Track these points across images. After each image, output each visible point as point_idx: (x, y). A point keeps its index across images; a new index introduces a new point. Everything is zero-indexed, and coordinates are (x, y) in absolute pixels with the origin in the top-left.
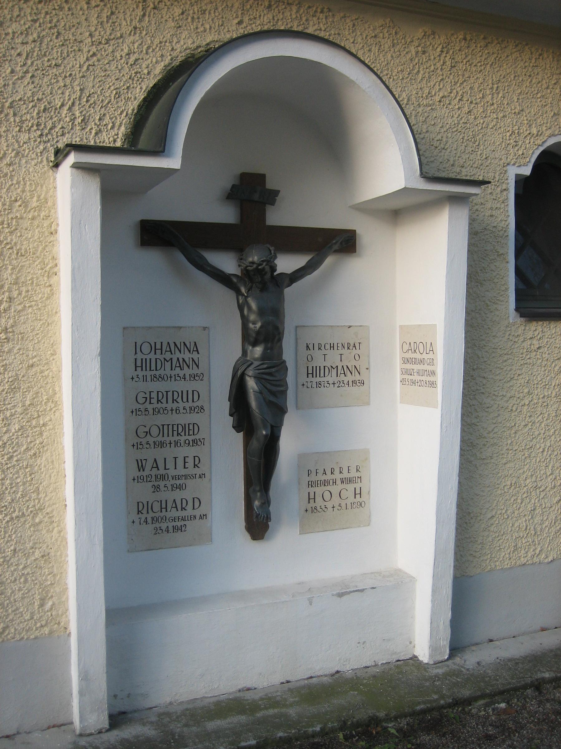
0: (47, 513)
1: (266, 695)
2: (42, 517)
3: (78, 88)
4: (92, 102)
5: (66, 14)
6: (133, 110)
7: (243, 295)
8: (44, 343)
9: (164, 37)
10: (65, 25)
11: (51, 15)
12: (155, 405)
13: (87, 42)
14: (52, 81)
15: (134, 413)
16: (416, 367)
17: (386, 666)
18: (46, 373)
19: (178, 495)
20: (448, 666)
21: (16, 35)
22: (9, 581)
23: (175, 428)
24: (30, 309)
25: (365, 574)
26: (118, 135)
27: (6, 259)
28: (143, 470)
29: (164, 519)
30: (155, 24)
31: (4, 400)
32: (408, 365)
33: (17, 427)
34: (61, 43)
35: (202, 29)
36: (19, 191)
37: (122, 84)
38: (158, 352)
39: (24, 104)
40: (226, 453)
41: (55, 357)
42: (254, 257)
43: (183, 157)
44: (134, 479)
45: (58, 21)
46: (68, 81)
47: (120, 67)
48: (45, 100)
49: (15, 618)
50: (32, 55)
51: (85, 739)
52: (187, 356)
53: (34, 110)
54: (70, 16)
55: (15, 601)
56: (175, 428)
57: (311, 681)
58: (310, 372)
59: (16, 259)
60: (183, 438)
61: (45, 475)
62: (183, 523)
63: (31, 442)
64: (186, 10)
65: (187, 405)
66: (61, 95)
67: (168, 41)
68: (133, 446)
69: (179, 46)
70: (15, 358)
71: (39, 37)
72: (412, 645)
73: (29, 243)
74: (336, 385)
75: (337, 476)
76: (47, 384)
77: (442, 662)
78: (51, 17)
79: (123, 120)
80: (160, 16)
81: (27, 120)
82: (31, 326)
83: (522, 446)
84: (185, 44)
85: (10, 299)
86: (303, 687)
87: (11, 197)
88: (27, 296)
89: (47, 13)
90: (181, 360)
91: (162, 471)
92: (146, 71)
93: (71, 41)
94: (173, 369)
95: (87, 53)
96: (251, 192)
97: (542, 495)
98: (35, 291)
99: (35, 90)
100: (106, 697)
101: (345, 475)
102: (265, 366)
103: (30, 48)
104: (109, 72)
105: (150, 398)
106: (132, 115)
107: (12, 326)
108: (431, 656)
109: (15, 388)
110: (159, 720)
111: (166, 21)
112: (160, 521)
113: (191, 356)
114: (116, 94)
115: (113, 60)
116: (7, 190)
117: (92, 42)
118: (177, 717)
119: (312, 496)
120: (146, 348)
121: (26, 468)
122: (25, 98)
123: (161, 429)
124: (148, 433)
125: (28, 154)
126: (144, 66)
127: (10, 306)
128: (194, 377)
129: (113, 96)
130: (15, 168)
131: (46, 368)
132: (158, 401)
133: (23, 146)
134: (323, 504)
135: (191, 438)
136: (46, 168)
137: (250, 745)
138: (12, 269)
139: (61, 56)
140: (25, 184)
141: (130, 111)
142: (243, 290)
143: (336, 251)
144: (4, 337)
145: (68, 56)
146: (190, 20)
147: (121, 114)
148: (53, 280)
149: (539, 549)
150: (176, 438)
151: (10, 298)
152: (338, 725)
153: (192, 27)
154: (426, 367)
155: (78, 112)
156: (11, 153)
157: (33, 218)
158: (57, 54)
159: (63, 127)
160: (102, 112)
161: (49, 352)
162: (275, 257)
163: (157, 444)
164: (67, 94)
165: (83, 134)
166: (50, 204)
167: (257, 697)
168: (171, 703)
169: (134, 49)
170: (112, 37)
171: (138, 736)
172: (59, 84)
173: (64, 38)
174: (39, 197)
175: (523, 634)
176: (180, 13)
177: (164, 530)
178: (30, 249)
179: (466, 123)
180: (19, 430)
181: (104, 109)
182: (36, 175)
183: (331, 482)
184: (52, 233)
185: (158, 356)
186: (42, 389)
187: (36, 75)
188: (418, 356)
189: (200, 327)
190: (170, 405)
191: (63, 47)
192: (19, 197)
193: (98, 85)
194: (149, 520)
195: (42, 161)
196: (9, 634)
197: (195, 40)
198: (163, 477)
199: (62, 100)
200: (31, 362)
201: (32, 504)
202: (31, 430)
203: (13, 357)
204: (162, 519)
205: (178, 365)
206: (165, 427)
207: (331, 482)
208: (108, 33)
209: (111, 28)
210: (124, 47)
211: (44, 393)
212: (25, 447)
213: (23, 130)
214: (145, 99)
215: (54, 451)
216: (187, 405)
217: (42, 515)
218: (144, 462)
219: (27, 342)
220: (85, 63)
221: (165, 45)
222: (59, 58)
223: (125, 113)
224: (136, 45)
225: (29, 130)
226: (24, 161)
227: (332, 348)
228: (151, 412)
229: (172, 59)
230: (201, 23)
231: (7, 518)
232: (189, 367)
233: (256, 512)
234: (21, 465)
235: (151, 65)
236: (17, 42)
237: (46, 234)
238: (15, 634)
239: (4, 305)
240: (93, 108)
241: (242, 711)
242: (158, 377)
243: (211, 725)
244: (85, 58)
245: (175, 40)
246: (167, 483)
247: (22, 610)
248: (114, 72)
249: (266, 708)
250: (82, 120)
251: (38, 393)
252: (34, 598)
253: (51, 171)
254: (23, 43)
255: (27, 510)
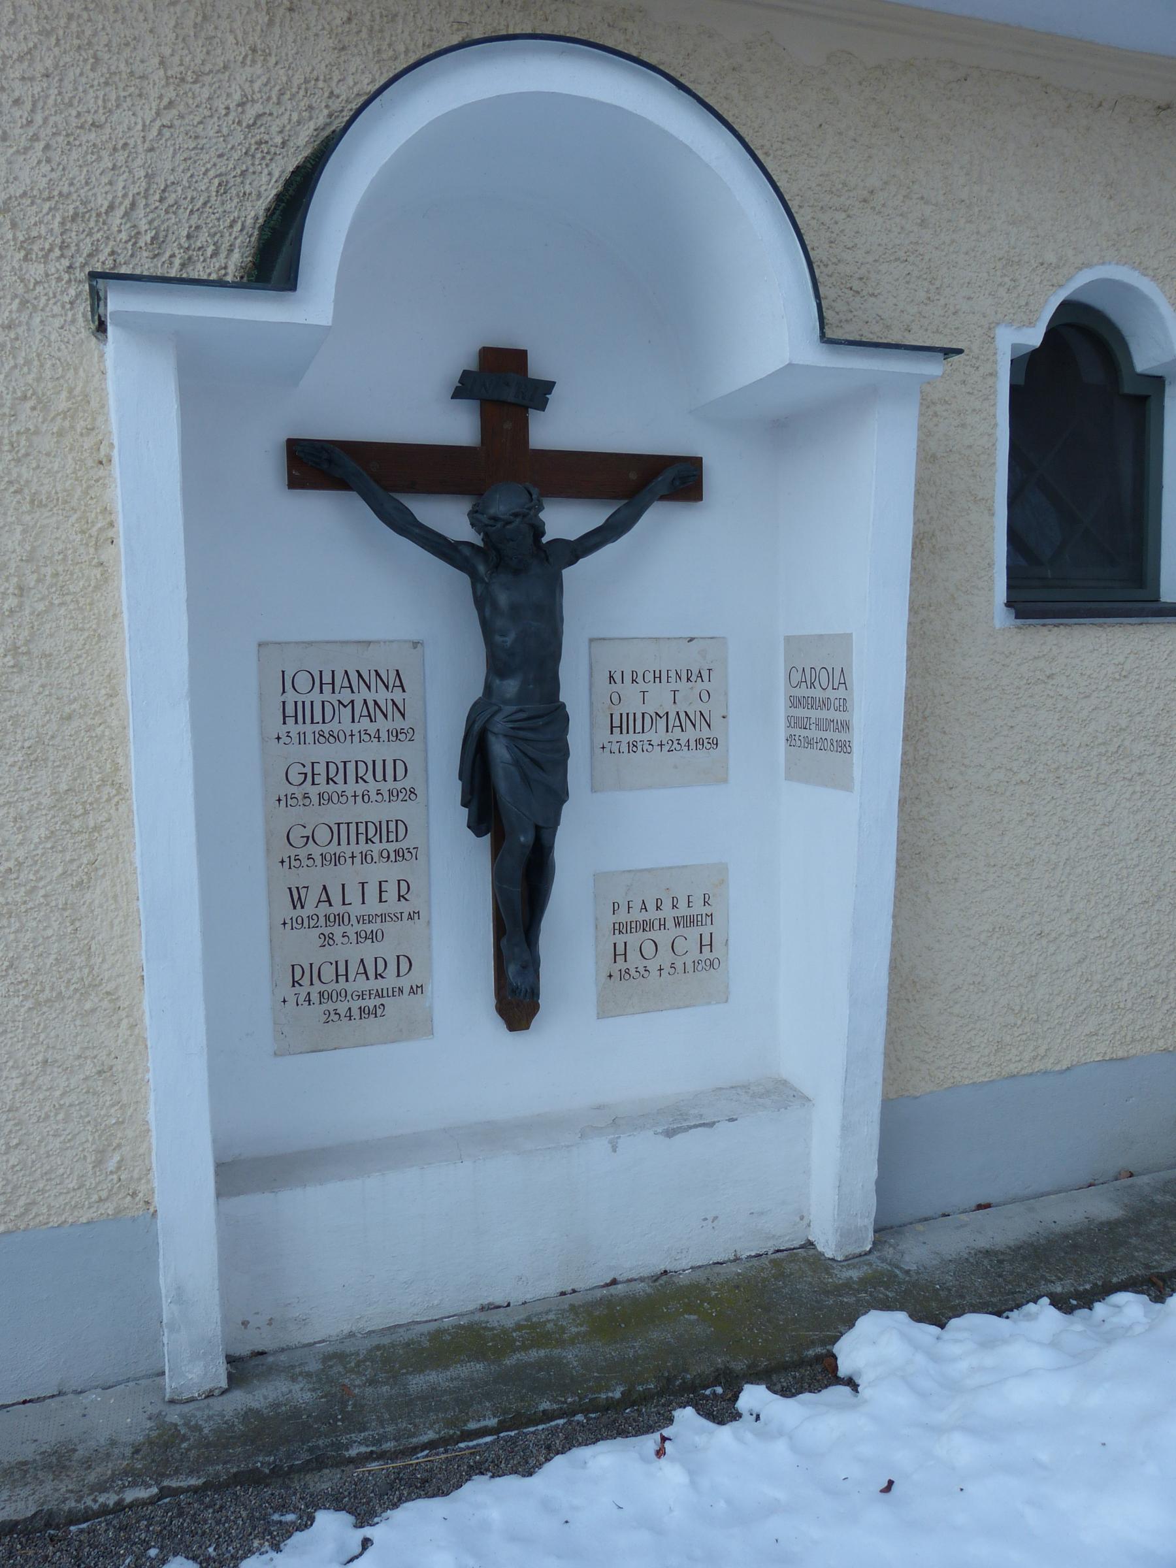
0: (108, 993)
1: (528, 1319)
2: (96, 1000)
3: (142, 173)
4: (171, 201)
5: (112, 19)
6: (256, 218)
7: (483, 581)
8: (92, 673)
9: (313, 70)
10: (110, 41)
11: (81, 21)
12: (323, 787)
13: (156, 78)
14: (89, 157)
15: (283, 803)
16: (814, 714)
17: (755, 1262)
18: (99, 730)
19: (368, 951)
20: (870, 1264)
21: (10, 62)
22: (34, 1119)
23: (362, 829)
24: (63, 609)
25: (721, 1089)
26: (225, 268)
27: (9, 513)
28: (302, 907)
29: (343, 994)
30: (295, 41)
31: (16, 783)
32: (801, 709)
33: (43, 832)
34: (102, 80)
35: (391, 53)
36: (30, 379)
37: (231, 166)
38: (327, 689)
39: (33, 203)
40: (456, 876)
41: (114, 700)
42: (502, 505)
43: (337, 302)
44: (284, 924)
45: (95, 34)
46: (121, 157)
47: (225, 131)
48: (75, 196)
49: (48, 1188)
50: (45, 103)
51: (178, 1408)
52: (382, 696)
53: (54, 216)
54: (118, 24)
55: (48, 1156)
56: (362, 829)
57: (613, 1290)
58: (616, 723)
59: (30, 512)
60: (376, 848)
61: (102, 921)
62: (378, 1001)
63: (72, 861)
64: (356, 14)
65: (385, 787)
66: (108, 188)
67: (322, 78)
68: (282, 862)
69: (344, 88)
70: (36, 704)
71: (56, 66)
72: (805, 1222)
73: (54, 480)
74: (666, 748)
75: (667, 912)
76: (100, 751)
77: (860, 1256)
78: (79, 25)
79: (236, 238)
80: (304, 26)
81: (39, 237)
82: (65, 641)
83: (1014, 859)
84: (355, 84)
85: (21, 590)
86: (600, 1302)
87: (14, 392)
88: (56, 584)
89: (70, 17)
90: (371, 705)
91: (338, 908)
92: (279, 140)
93: (124, 76)
94: (356, 720)
95: (157, 102)
96: (502, 383)
97: (1052, 949)
98: (72, 574)
99: (54, 175)
100: (219, 1333)
101: (683, 910)
102: (524, 715)
103: (39, 89)
104: (205, 141)
105: (313, 775)
106: (254, 228)
107: (27, 642)
108: (840, 1246)
109: (36, 760)
110: (323, 1370)
111: (316, 35)
112: (334, 999)
113: (390, 696)
114: (220, 185)
115: (211, 116)
116: (6, 376)
117: (167, 78)
118: (358, 1365)
119: (620, 950)
120: (303, 682)
121: (64, 909)
122: (35, 193)
123: (335, 831)
124: (310, 839)
125: (46, 305)
126: (275, 129)
127: (21, 606)
128: (397, 734)
129: (214, 188)
130: (21, 333)
131: (97, 721)
132: (328, 779)
133: (34, 289)
134: (641, 964)
135: (392, 847)
136: (84, 334)
137: (486, 1427)
138: (24, 531)
139: (105, 108)
140: (42, 366)
141: (249, 221)
142: (481, 569)
143: (663, 498)
144: (11, 663)
145: (118, 106)
146: (364, 35)
147: (231, 226)
148: (107, 554)
149: (1045, 1047)
150: (363, 847)
151: (21, 589)
152: (656, 1387)
153: (370, 48)
154: (831, 714)
155: (144, 221)
156: (10, 304)
157: (61, 434)
158: (96, 102)
159: (113, 253)
160: (193, 222)
161: (103, 692)
162: (541, 508)
163: (328, 858)
164: (121, 184)
165: (156, 267)
166: (94, 404)
167: (509, 1323)
168: (351, 1335)
169: (254, 93)
170: (207, 69)
171: (279, 1405)
172: (103, 165)
173: (109, 69)
174: (71, 391)
175: (1013, 1201)
176: (345, 19)
177: (342, 1015)
178: (56, 493)
179: (917, 243)
180: (47, 838)
181: (196, 216)
182: (63, 347)
183: (656, 924)
184: (101, 463)
185: (327, 695)
186: (91, 761)
187: (55, 145)
188: (817, 693)
189: (405, 641)
190: (352, 787)
191: (108, 89)
192: (30, 392)
193: (182, 167)
194: (315, 997)
195: (73, 321)
196: (37, 1215)
197: (377, 76)
198: (340, 919)
199: (110, 197)
200: (67, 710)
201: (78, 975)
202: (72, 838)
203: (31, 701)
204: (339, 994)
205: (365, 713)
206: (343, 828)
207: (656, 924)
208: (198, 61)
209: (205, 50)
210: (232, 90)
211: (96, 769)
212: (60, 870)
213: (34, 257)
214: (279, 197)
215: (119, 877)
216: (385, 787)
217: (97, 995)
218: (303, 892)
219: (58, 673)
220: (153, 121)
221: (315, 87)
222: (101, 111)
223: (239, 224)
224: (257, 86)
225: (46, 256)
226: (37, 320)
227: (657, 680)
228: (315, 799)
229: (330, 116)
230: (388, 40)
231: (29, 1004)
232: (386, 716)
233: (511, 984)
234: (53, 904)
235: (288, 127)
236: (12, 76)
237: (90, 463)
238: (49, 1215)
239: (12, 602)
240: (175, 213)
241: (479, 1354)
242: (327, 735)
243: (418, 1383)
244: (154, 111)
245: (336, 76)
246: (348, 929)
247: (61, 1171)
248: (214, 141)
249: (525, 1348)
250: (153, 238)
251: (84, 768)
252: (83, 1150)
253: (94, 340)
254: (23, 79)
255: (67, 987)
